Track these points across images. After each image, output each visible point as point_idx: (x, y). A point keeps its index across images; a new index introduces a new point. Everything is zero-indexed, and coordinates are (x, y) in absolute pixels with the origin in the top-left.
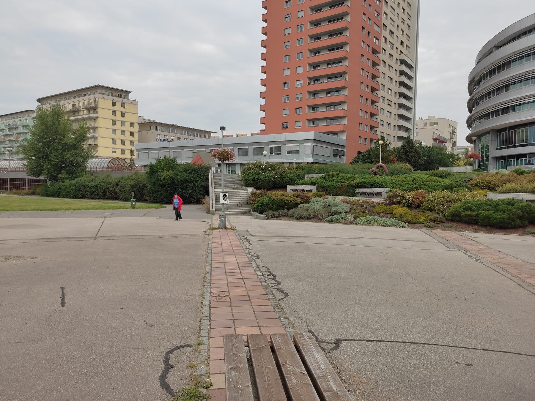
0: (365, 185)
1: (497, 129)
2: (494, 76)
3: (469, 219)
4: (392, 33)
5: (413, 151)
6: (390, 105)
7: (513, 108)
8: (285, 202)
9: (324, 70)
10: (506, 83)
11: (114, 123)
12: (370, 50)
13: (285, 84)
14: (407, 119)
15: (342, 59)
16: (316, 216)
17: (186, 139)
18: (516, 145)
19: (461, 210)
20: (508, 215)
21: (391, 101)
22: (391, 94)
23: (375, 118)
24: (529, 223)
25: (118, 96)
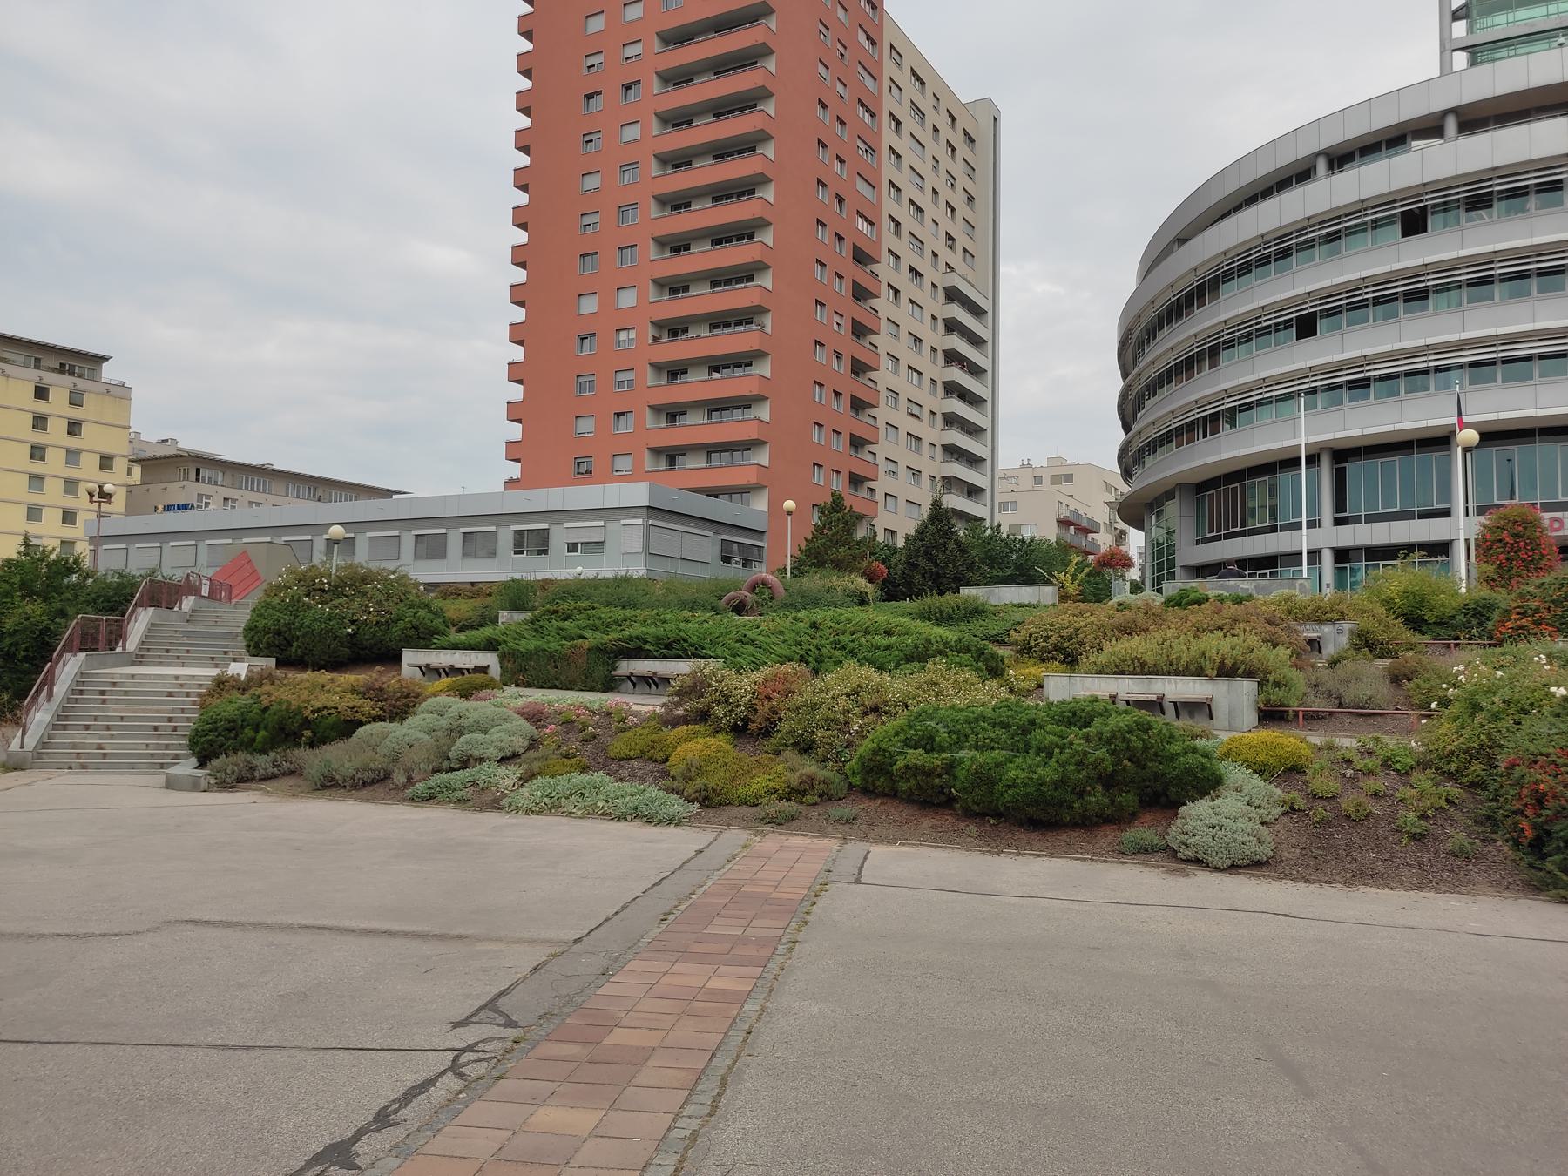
0: (647, 647)
1: (1196, 482)
2: (1180, 323)
3: (919, 787)
4: (919, 209)
5: (951, 545)
6: (916, 416)
7: (1231, 416)
8: (307, 717)
9: (702, 300)
10: (1210, 342)
11: (37, 453)
12: (847, 251)
13: (583, 338)
14: (973, 461)
15: (752, 270)
16: (384, 777)
17: (259, 504)
18: (1247, 528)
19: (895, 746)
20: (1061, 770)
21: (921, 406)
22: (919, 386)
23: (869, 452)
24: (1141, 801)
25: (62, 369)
